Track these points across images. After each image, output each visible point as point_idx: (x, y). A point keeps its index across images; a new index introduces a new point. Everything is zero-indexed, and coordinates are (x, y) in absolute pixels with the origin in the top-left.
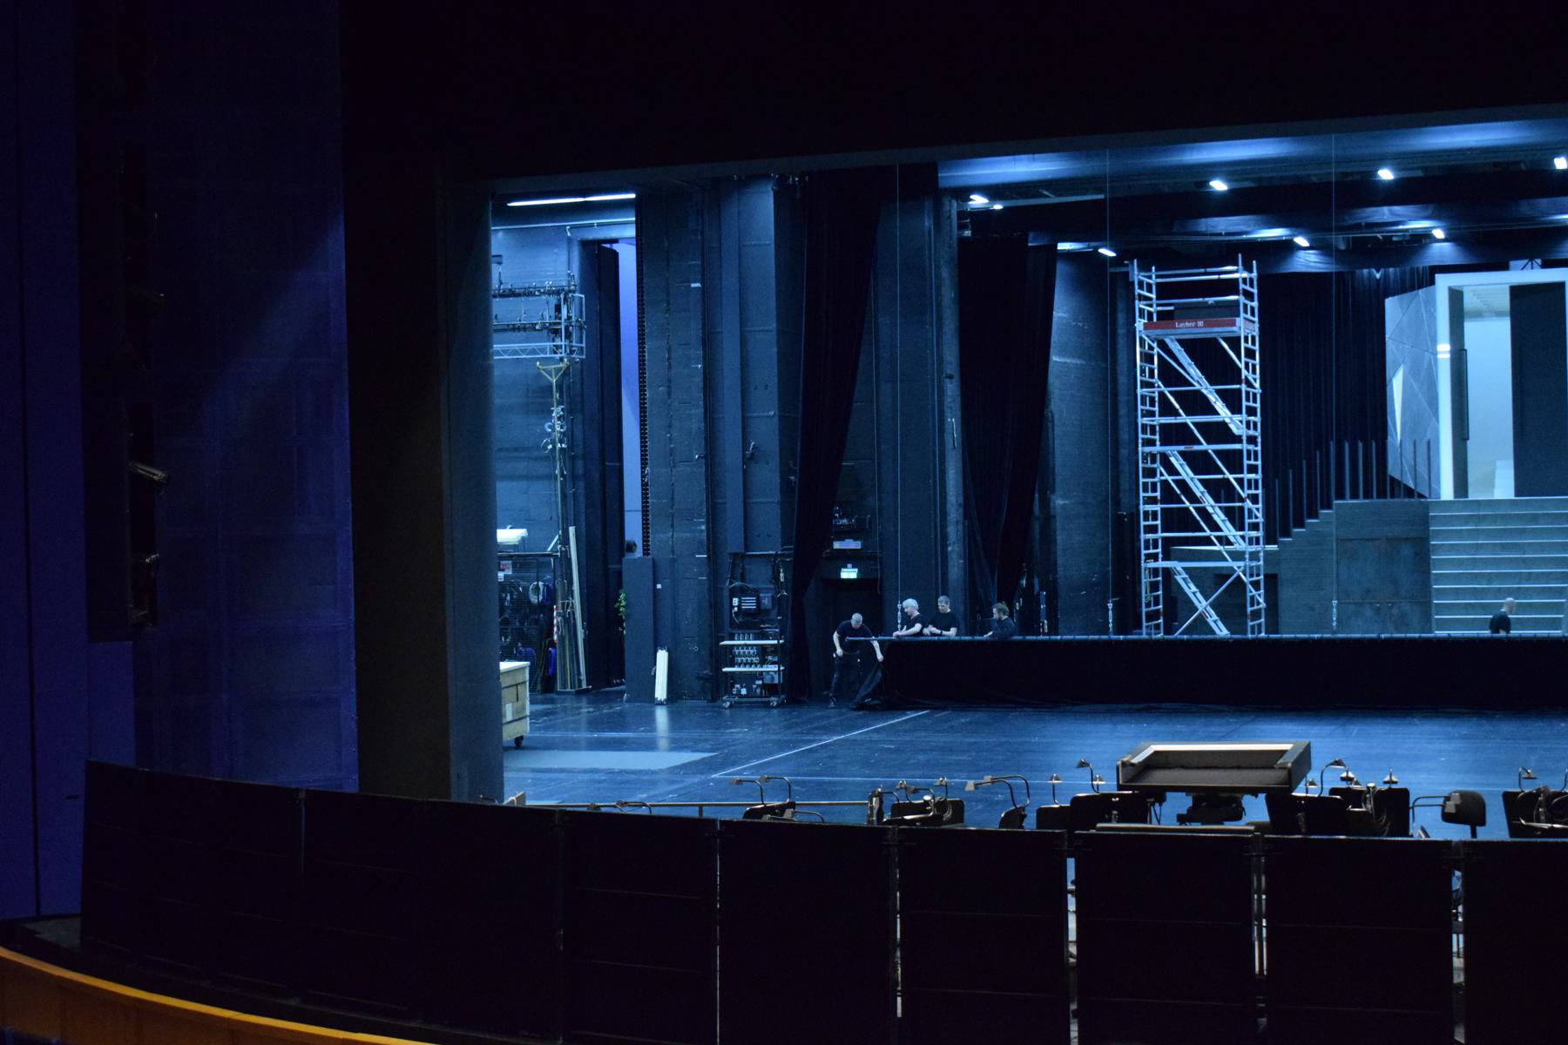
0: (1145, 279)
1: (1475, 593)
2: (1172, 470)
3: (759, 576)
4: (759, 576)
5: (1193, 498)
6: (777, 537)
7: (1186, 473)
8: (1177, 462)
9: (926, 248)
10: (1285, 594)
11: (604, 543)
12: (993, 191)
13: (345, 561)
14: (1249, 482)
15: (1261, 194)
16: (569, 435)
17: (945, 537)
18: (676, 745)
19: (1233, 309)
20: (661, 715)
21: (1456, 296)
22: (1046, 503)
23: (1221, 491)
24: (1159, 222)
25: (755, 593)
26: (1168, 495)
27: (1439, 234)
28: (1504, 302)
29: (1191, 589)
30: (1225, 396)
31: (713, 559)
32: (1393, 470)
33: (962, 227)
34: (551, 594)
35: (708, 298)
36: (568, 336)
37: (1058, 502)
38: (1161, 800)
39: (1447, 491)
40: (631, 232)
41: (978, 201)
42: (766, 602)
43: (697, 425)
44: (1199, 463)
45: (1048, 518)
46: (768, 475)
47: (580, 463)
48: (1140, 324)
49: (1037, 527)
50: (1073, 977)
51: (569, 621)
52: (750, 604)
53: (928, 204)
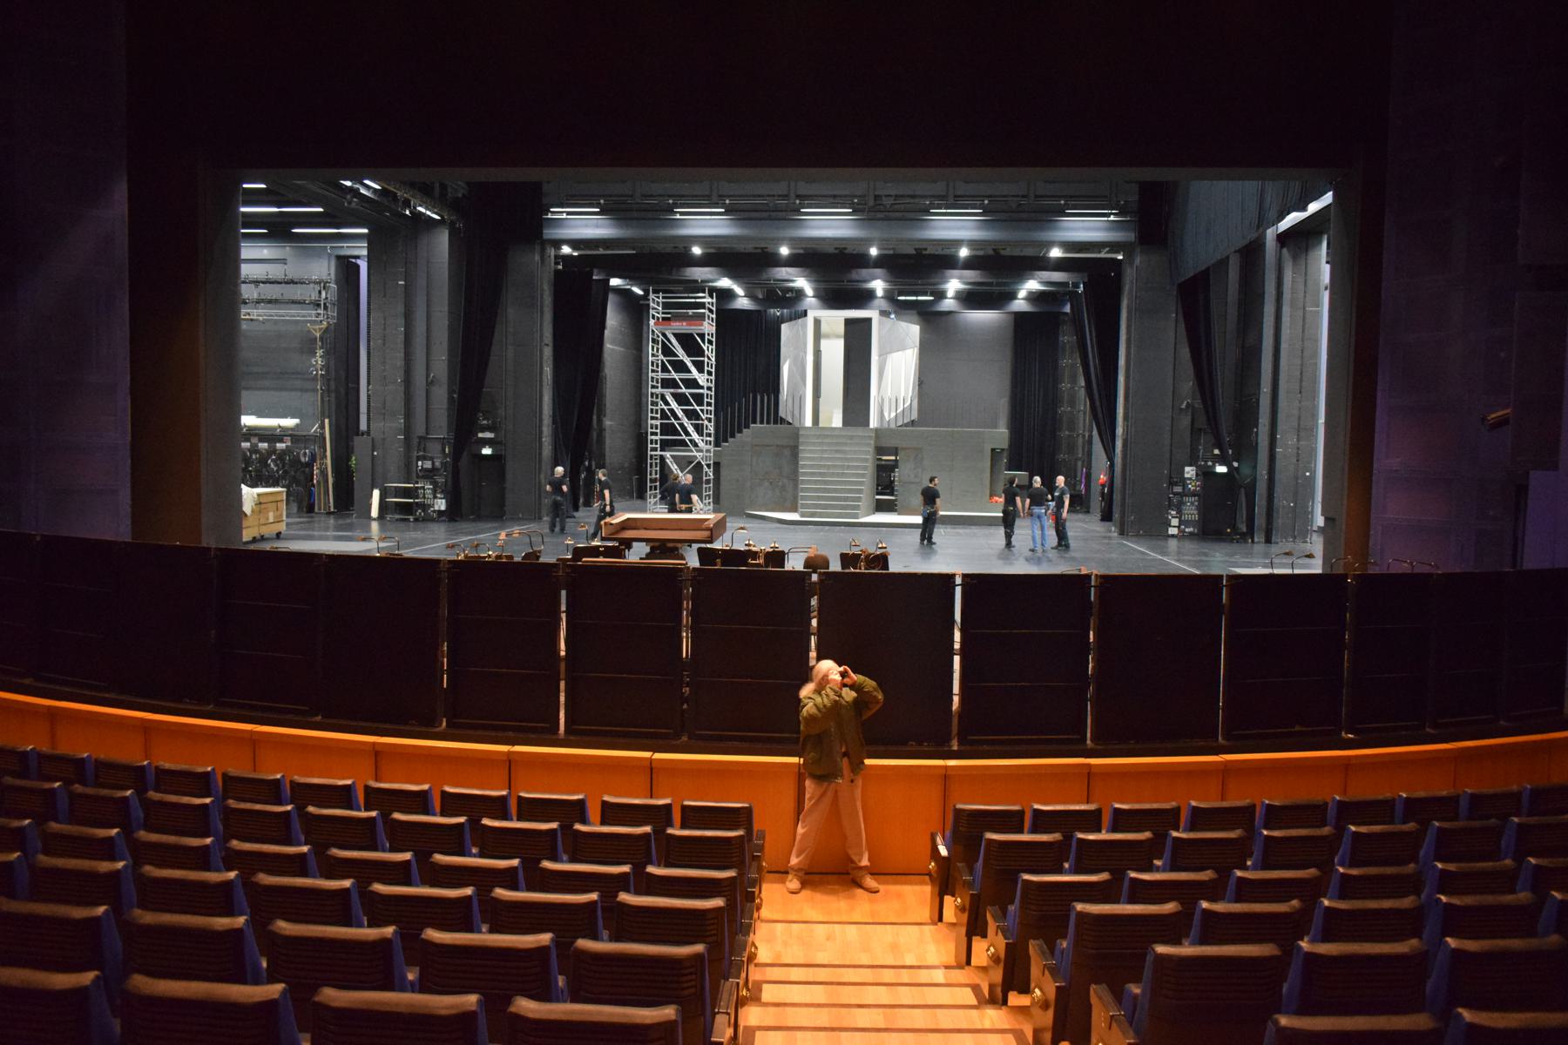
0: (656, 304)
1: (821, 474)
2: (667, 403)
3: (434, 449)
4: (434, 449)
5: (676, 418)
6: (445, 429)
7: (674, 405)
8: (669, 399)
9: (536, 274)
10: (724, 472)
11: (346, 430)
12: (574, 243)
13: (124, 402)
14: (707, 412)
15: (722, 257)
16: (326, 367)
17: (541, 432)
18: (383, 539)
19: (702, 317)
20: (375, 526)
21: (817, 322)
22: (600, 421)
23: (692, 415)
24: (662, 266)
25: (432, 459)
26: (664, 415)
27: (809, 291)
28: (841, 329)
29: (674, 467)
30: (696, 364)
31: (407, 439)
32: (782, 414)
33: (557, 263)
34: (313, 458)
35: (408, 292)
36: (326, 308)
37: (607, 423)
38: (629, 547)
39: (808, 422)
40: (365, 252)
41: (566, 250)
42: (437, 464)
43: (400, 363)
44: (681, 399)
45: (601, 430)
46: (441, 394)
47: (332, 384)
48: (652, 322)
49: (595, 435)
50: (563, 666)
51: (323, 473)
52: (428, 465)
53: (538, 248)
